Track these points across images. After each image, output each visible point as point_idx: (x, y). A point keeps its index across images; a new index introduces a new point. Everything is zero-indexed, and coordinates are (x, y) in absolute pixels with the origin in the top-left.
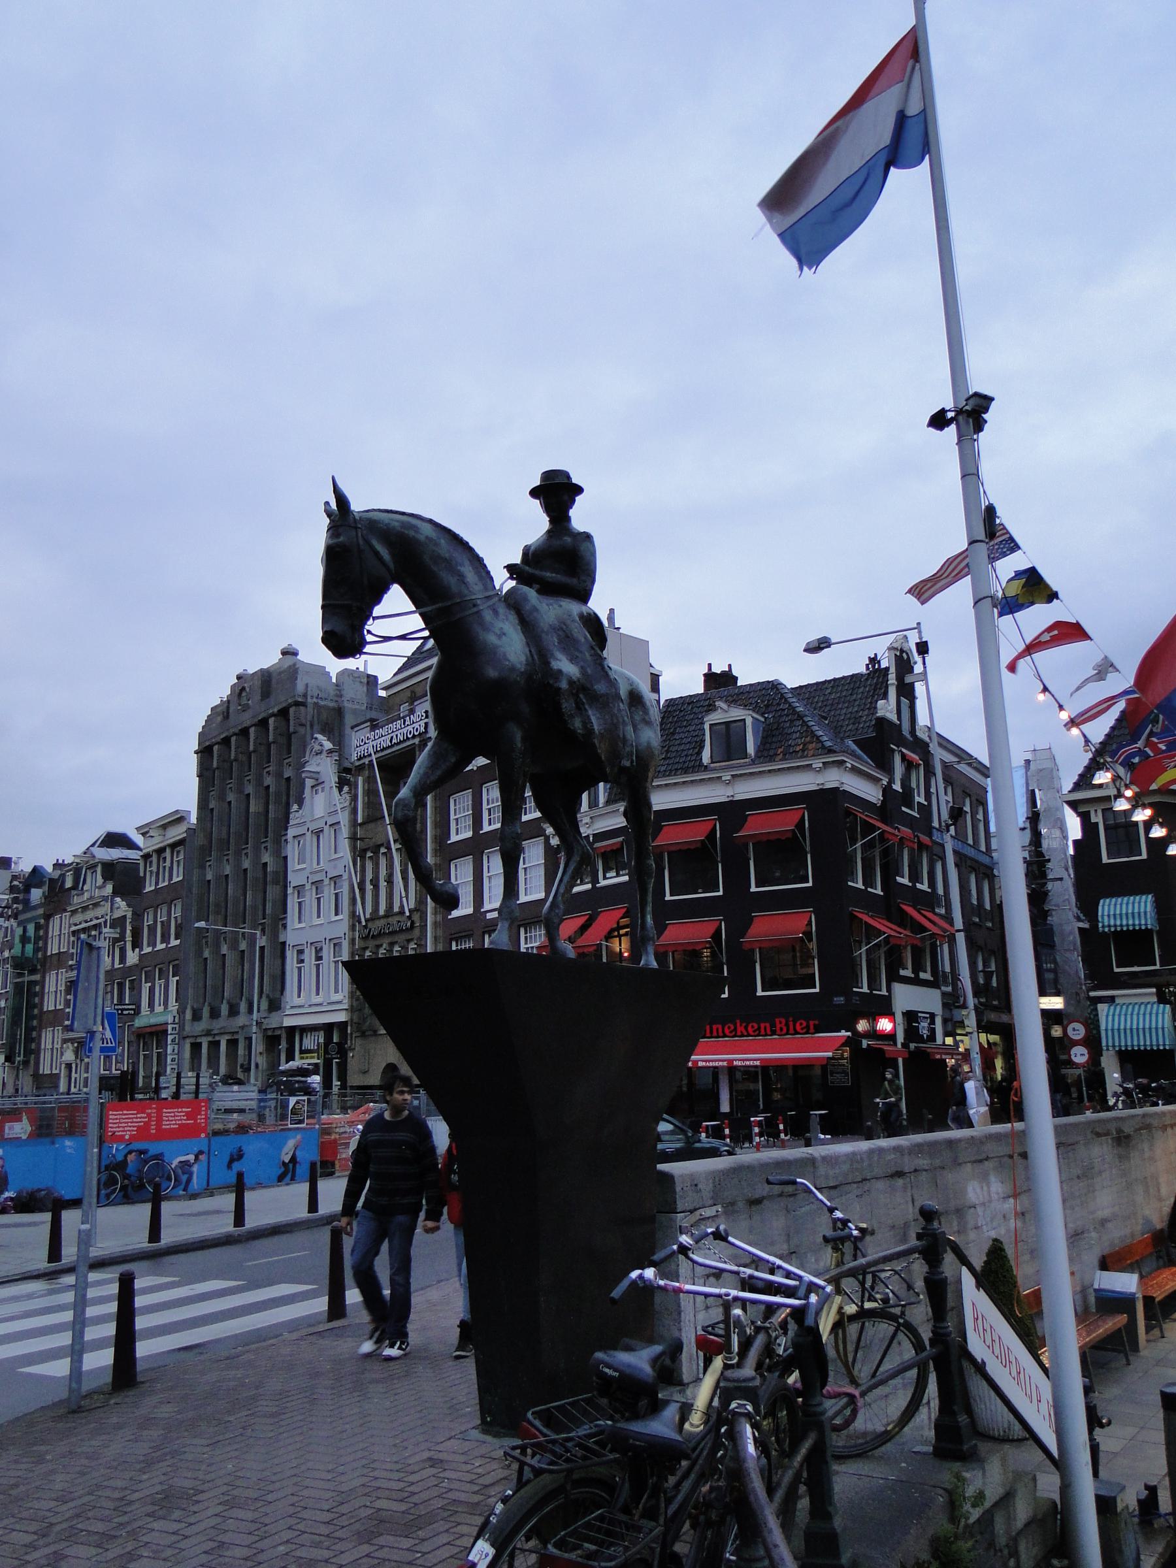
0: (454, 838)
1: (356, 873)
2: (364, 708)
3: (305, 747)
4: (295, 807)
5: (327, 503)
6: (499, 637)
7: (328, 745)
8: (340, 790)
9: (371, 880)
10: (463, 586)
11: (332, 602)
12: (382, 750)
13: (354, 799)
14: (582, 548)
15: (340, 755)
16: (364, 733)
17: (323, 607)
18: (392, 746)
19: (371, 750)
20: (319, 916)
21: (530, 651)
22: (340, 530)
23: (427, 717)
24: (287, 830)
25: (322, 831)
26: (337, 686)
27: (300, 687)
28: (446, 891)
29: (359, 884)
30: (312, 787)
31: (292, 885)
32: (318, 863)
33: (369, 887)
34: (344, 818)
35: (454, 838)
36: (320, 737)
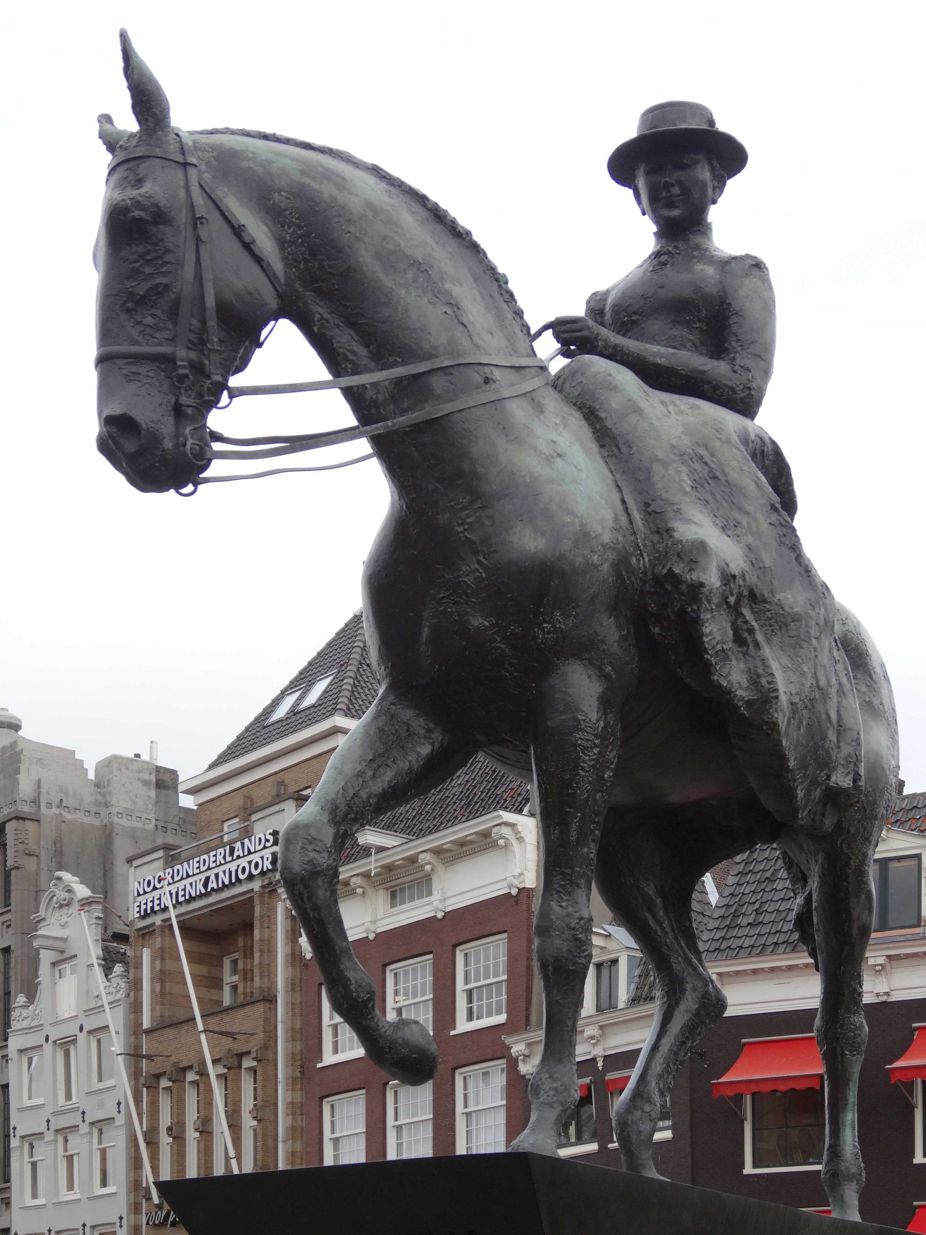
0: (329, 1058)
1: (140, 1115)
2: (151, 827)
3: (38, 892)
4: (21, 999)
5: (106, 119)
6: (549, 460)
7: (82, 891)
8: (107, 971)
9: (170, 1129)
10: (459, 332)
11: (126, 348)
12: (188, 902)
13: (136, 986)
14: (742, 293)
15: (105, 910)
16: (153, 869)
17: (103, 361)
18: (207, 894)
19: (167, 901)
20: (71, 1187)
21: (623, 502)
22: (143, 169)
23: (276, 843)
24: (6, 1039)
25: (74, 1041)
26: (97, 785)
27: (25, 788)
28: (406, 1043)
29: (145, 1135)
30: (54, 964)
31: (19, 1133)
32: (69, 1096)
33: (165, 1140)
34: (115, 1019)
35: (329, 1058)
36: (66, 876)
